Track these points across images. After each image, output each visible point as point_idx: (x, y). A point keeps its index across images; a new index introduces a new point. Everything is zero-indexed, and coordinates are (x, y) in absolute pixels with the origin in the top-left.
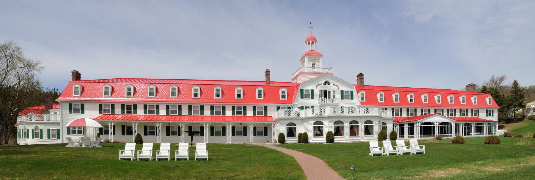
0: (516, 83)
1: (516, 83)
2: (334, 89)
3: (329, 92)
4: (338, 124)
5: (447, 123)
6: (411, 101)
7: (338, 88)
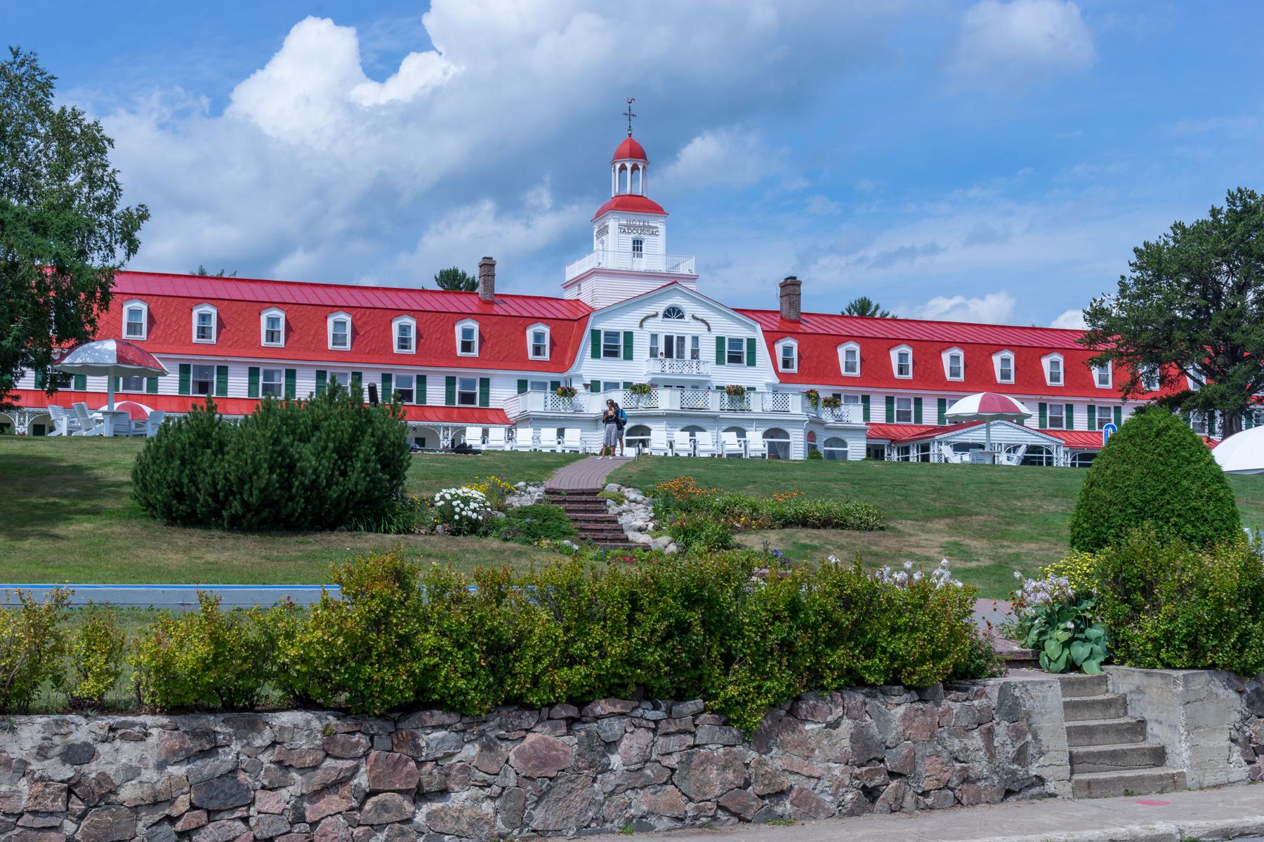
2: (696, 333)
3: (681, 340)
4: (642, 435)
6: (901, 372)
7: (709, 329)
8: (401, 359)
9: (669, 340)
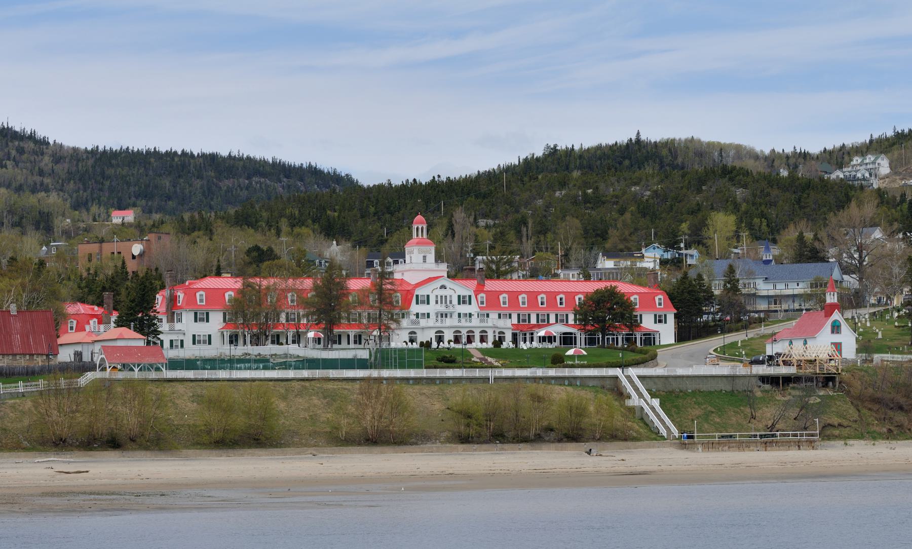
0: (86, 148)
1: (86, 148)
3: (446, 297)
5: (571, 334)
6: (542, 304)
8: (505, 309)
9: (441, 297)
